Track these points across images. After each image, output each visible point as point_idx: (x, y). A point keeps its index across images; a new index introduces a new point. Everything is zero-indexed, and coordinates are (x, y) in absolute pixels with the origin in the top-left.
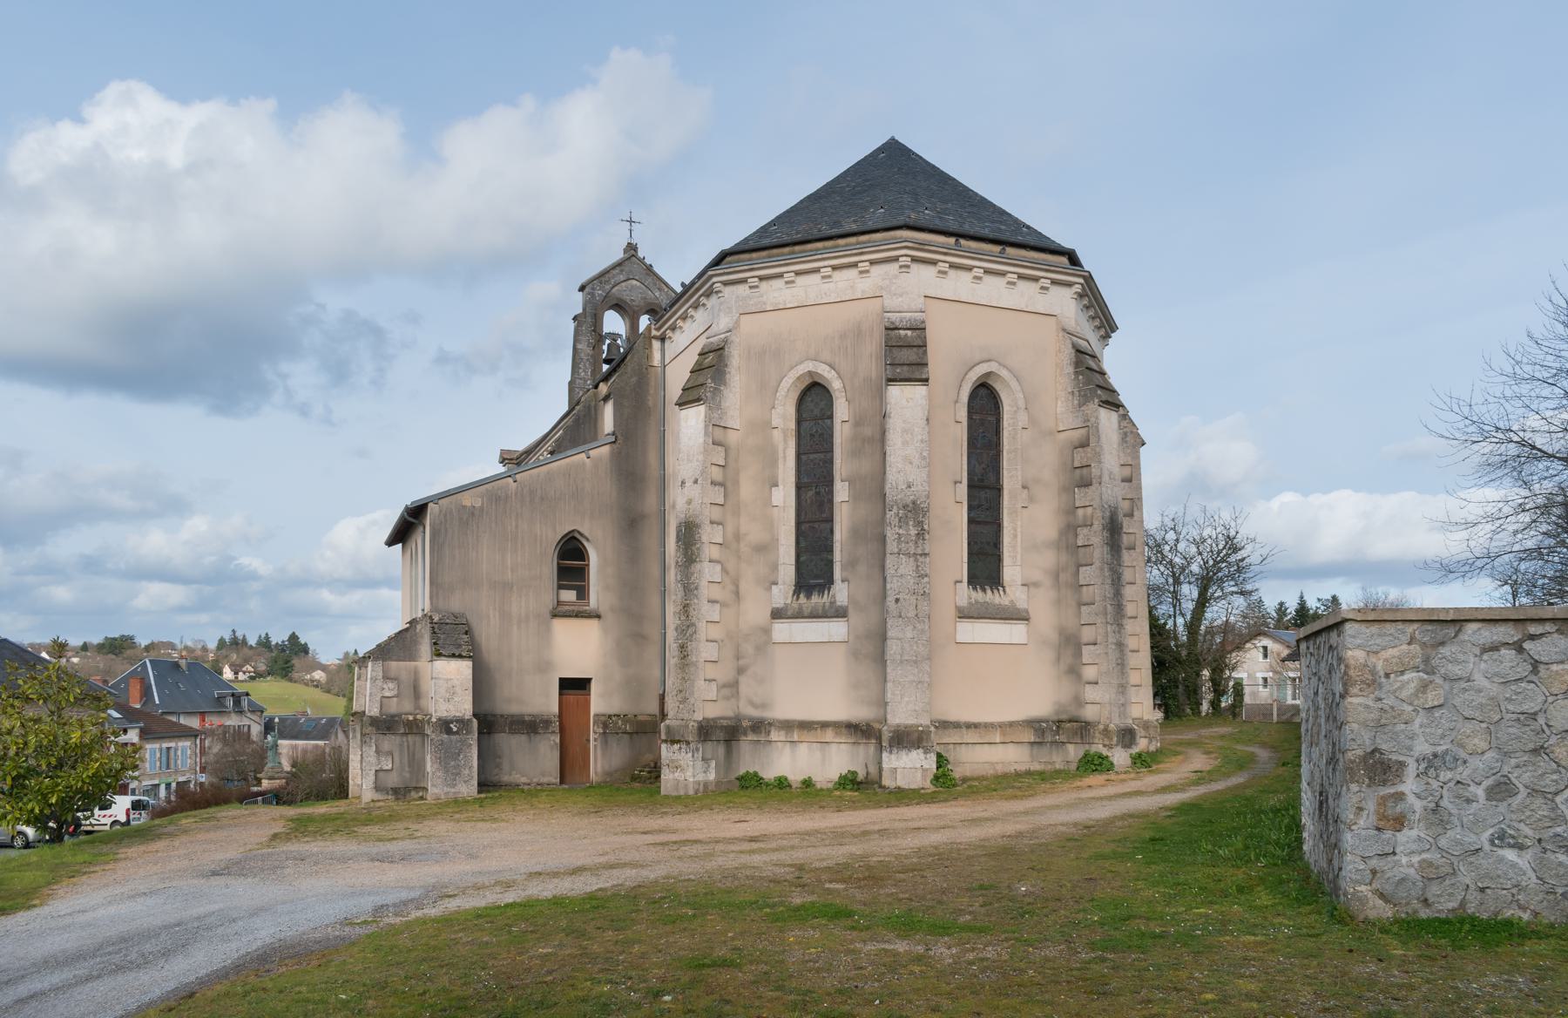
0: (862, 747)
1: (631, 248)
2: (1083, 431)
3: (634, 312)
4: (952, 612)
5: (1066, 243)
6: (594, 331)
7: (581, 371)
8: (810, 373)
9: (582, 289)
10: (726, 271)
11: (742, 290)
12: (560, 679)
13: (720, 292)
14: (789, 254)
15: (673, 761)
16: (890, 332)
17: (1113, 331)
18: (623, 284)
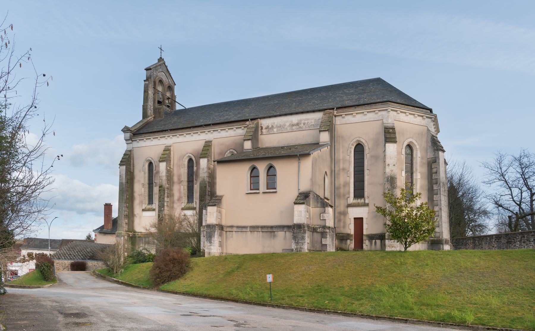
0: (424, 244)
1: (161, 59)
2: (435, 158)
3: (165, 85)
4: (370, 205)
5: (429, 106)
6: (154, 88)
7: (150, 102)
8: (358, 141)
9: (147, 69)
10: (395, 107)
11: (394, 113)
12: (355, 218)
13: (390, 112)
14: (381, 105)
15: (391, 245)
16: (386, 129)
17: (439, 133)
18: (161, 73)
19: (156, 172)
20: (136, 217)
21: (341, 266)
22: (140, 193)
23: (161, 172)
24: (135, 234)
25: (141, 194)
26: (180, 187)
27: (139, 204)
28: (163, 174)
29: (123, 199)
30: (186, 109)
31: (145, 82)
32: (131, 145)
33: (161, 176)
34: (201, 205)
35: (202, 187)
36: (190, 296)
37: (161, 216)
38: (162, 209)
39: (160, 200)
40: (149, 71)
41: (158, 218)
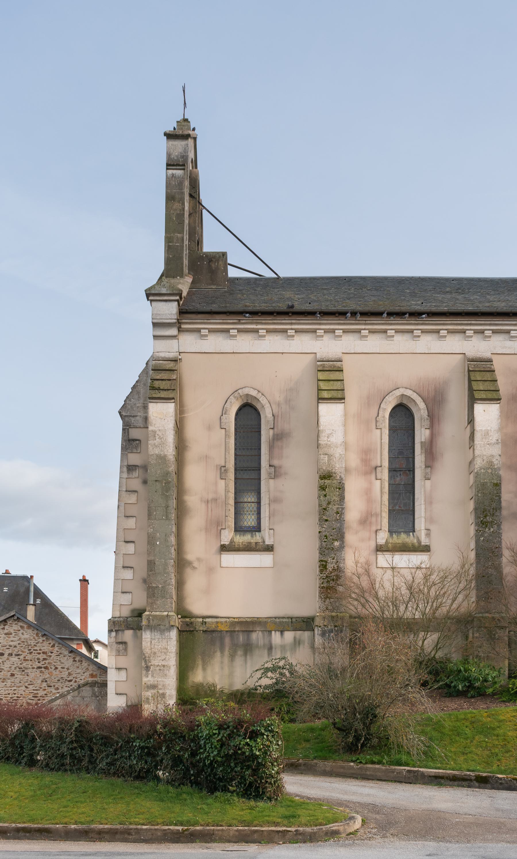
19: (274, 435)
20: (194, 568)
21: (88, 791)
22: (211, 496)
23: (328, 432)
24: (191, 623)
25: (215, 500)
26: (371, 483)
27: (207, 530)
28: (333, 439)
29: (167, 507)
30: (279, 278)
31: (170, 172)
32: (174, 343)
33: (328, 446)
34: (482, 535)
35: (484, 485)
36: (8, 838)
37: (330, 567)
38: (336, 544)
39: (325, 518)
40: (179, 144)
41: (321, 571)
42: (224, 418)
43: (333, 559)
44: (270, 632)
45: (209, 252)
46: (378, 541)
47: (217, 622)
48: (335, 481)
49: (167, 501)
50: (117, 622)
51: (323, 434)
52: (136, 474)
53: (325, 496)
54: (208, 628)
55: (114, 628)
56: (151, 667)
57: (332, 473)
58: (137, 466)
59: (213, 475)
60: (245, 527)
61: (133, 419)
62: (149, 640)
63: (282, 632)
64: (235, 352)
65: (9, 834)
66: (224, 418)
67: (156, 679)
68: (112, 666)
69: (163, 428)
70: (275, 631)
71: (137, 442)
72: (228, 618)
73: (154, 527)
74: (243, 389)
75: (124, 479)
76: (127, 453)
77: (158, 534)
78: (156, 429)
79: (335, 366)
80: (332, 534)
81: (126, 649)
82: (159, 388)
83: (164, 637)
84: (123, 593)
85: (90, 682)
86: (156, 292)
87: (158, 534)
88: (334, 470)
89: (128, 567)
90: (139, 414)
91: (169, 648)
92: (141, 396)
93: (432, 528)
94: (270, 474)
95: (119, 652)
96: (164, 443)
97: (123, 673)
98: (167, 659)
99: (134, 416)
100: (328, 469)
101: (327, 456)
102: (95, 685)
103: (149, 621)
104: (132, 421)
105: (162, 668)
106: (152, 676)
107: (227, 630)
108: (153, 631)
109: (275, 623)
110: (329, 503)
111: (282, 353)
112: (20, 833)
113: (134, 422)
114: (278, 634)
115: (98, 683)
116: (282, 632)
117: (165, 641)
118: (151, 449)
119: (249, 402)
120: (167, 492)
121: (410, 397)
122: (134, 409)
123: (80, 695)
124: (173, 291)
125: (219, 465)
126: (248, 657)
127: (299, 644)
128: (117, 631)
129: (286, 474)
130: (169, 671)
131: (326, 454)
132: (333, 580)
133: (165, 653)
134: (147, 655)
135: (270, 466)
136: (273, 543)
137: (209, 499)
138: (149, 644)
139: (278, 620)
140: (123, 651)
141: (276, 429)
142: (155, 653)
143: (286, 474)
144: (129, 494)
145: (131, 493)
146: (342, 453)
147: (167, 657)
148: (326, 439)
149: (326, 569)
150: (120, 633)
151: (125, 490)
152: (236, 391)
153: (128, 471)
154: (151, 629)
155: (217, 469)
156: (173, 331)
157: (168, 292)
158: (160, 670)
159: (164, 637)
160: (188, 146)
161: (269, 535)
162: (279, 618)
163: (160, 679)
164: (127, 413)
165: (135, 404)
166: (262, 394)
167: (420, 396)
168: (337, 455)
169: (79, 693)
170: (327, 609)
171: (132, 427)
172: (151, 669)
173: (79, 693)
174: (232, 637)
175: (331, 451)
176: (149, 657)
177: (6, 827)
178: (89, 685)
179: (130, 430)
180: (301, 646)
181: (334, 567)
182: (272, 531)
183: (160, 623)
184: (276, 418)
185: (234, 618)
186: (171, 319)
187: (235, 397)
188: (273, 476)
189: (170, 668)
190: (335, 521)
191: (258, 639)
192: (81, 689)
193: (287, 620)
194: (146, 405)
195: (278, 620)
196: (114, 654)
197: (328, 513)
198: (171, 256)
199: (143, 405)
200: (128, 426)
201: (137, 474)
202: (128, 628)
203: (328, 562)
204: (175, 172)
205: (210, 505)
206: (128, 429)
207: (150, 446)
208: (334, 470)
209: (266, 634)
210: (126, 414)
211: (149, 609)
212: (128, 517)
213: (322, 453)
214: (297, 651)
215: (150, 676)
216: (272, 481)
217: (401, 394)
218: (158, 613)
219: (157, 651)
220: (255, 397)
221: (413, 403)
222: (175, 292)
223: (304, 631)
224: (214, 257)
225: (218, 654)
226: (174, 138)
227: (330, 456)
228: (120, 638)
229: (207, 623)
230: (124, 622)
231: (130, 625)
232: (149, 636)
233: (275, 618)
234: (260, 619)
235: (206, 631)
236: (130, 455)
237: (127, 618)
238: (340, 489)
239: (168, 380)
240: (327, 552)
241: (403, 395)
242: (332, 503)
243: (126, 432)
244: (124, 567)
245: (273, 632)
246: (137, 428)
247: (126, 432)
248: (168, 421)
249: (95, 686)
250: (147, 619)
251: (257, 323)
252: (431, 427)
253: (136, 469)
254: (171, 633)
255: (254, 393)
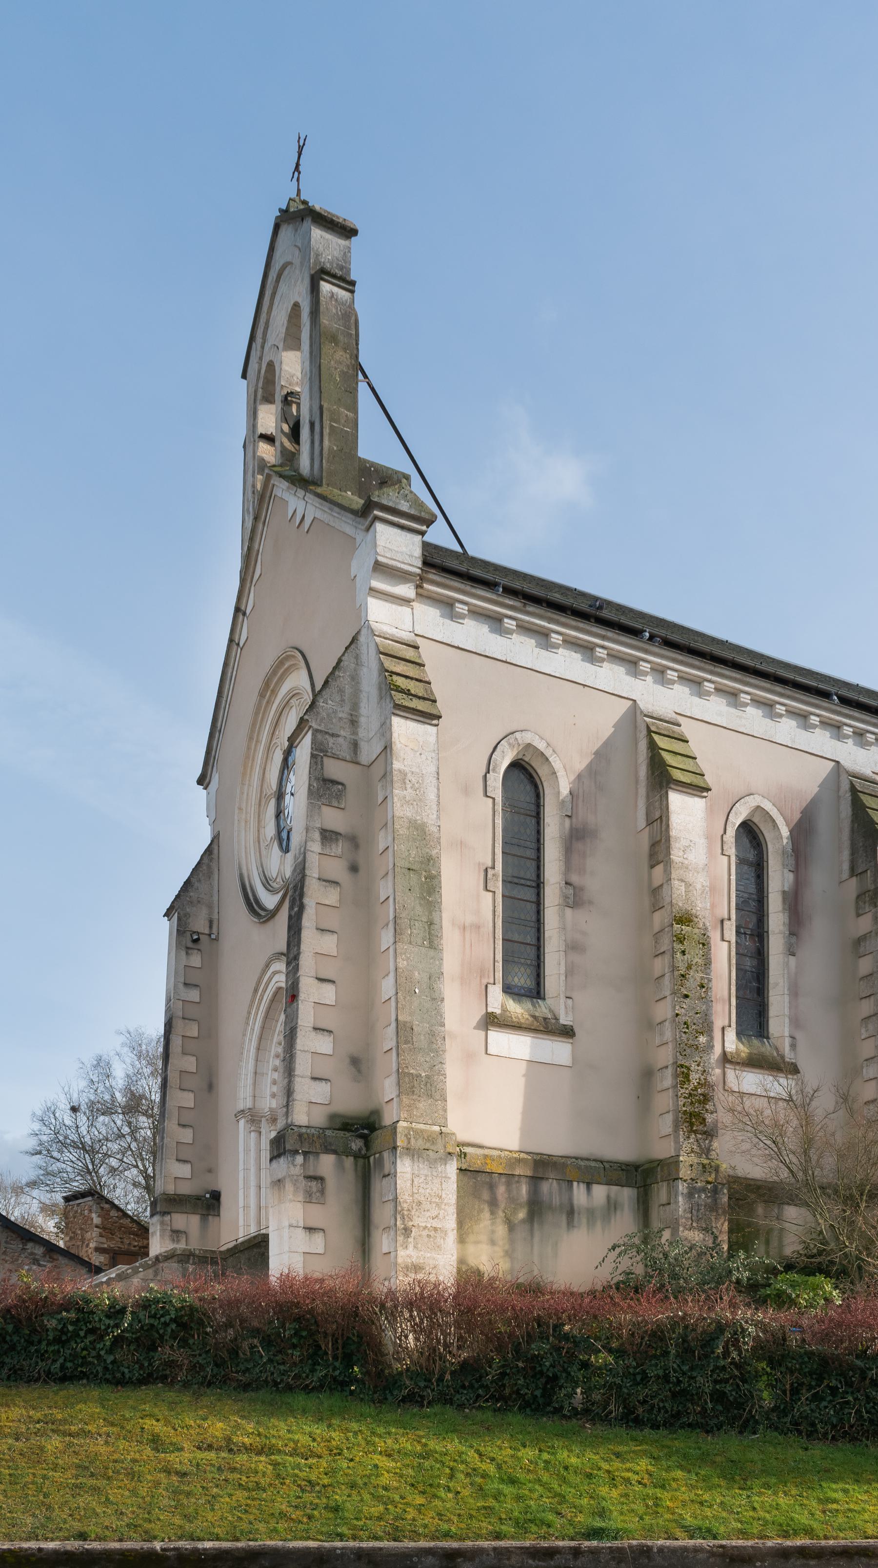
19: (571, 829)
37: (694, 1077)
38: (702, 1039)
42: (492, 778)
43: (698, 1065)
44: (570, 1182)
45: (382, 466)
46: (726, 1045)
47: (486, 1156)
48: (696, 931)
49: (430, 913)
50: (306, 1136)
51: (677, 845)
52: (338, 848)
53: (683, 953)
54: (470, 1166)
55: (301, 1148)
56: (414, 1230)
57: (692, 915)
58: (340, 834)
59: (475, 880)
60: (516, 986)
61: (331, 740)
62: (409, 1176)
63: (589, 1185)
64: (508, 660)
65: (758, 1564)
66: (492, 778)
67: (422, 1253)
68: (298, 1222)
69: (417, 770)
70: (578, 1182)
71: (340, 787)
72: (501, 1150)
73: (408, 958)
74: (523, 733)
75: (314, 855)
76: (320, 803)
77: (416, 974)
78: (407, 769)
79: (674, 732)
80: (695, 1021)
81: (322, 1191)
82: (409, 690)
83: (435, 1174)
84: (314, 1079)
85: (179, 1252)
86: (390, 504)
87: (416, 974)
88: (694, 911)
89: (323, 1030)
90: (342, 733)
91: (444, 1196)
92: (346, 698)
93: (799, 1036)
94: (566, 897)
95: (310, 1195)
96: (420, 800)
97: (319, 1238)
98: (441, 1216)
99: (333, 735)
100: (686, 906)
101: (683, 884)
102: (189, 1259)
103: (409, 1140)
104: (331, 745)
105: (432, 1233)
106: (415, 1247)
107: (502, 1172)
108: (416, 1159)
109: (579, 1168)
110: (689, 967)
111: (584, 686)
112: (792, 1560)
113: (334, 747)
114: (583, 1187)
115: (194, 1255)
116: (589, 1185)
117: (437, 1181)
118: (399, 805)
119: (527, 759)
120: (430, 894)
121: (768, 813)
122: (334, 721)
123: (159, 1278)
124: (420, 511)
125: (483, 864)
126: (536, 1226)
127: (615, 1208)
128: (305, 1154)
129: (591, 903)
130: (444, 1239)
131: (682, 881)
132: (699, 1102)
133: (437, 1205)
134: (405, 1206)
135: (566, 883)
136: (571, 1023)
137: (467, 924)
138: (409, 1184)
139: (582, 1163)
140: (318, 1194)
141: (574, 820)
142: (419, 1203)
143: (591, 903)
144: (325, 887)
145: (327, 884)
146: (705, 883)
147: (442, 1212)
148: (681, 854)
149: (689, 1081)
150: (311, 1157)
151: (317, 876)
152: (512, 733)
153: (322, 839)
154: (413, 1156)
155: (479, 871)
156: (407, 590)
157: (413, 512)
158: (429, 1236)
159: (435, 1174)
160: (349, 252)
161: (566, 1007)
162: (582, 1159)
163: (429, 1255)
164: (320, 725)
165: (335, 712)
166: (554, 751)
167: (782, 815)
168: (699, 886)
169: (156, 1274)
170: (692, 1152)
171: (329, 754)
172: (413, 1234)
173: (156, 1274)
174: (508, 1184)
175: (690, 877)
176: (409, 1210)
177: (752, 1547)
178: (176, 1258)
179: (325, 760)
180: (618, 1213)
181: (700, 1079)
182: (569, 1001)
183: (427, 1146)
184: (575, 799)
185: (511, 1152)
186: (410, 565)
187: (510, 744)
188: (571, 901)
189: (446, 1234)
190: (698, 999)
191: (551, 1194)
192: (161, 1265)
193: (593, 1164)
194: (354, 718)
195: (582, 1163)
196: (301, 1198)
197: (688, 984)
198: (335, 448)
199: (349, 717)
200: (321, 751)
201: (340, 850)
202: (328, 1149)
203: (692, 1069)
204: (335, 290)
205: (467, 934)
206: (322, 758)
207: (396, 799)
208: (694, 911)
209: (564, 1185)
210: (319, 728)
211: (406, 1115)
212: (323, 930)
213: (676, 878)
214: (613, 1221)
215: (411, 1247)
216: (568, 911)
217: (756, 804)
218: (422, 1126)
219: (423, 1199)
220: (542, 753)
221: (770, 824)
222: (423, 515)
223: (623, 1186)
224: (390, 477)
225: (486, 1214)
226: (325, 226)
227: (688, 885)
228: (312, 1168)
229: (468, 1157)
230: (319, 1137)
231: (330, 1144)
232: (409, 1169)
233: (577, 1158)
234: (554, 1159)
235: (465, 1170)
236: (326, 810)
237: (324, 1129)
238: (704, 945)
239: (417, 680)
240: (688, 1050)
241: (758, 807)
242: (694, 968)
243: (319, 763)
244: (315, 1029)
245: (575, 1184)
246: (338, 759)
247: (319, 763)
248: (427, 759)
249: (187, 1262)
250: (406, 1135)
251: (550, 620)
252: (797, 870)
253: (337, 840)
254: (448, 1166)
255: (541, 746)
